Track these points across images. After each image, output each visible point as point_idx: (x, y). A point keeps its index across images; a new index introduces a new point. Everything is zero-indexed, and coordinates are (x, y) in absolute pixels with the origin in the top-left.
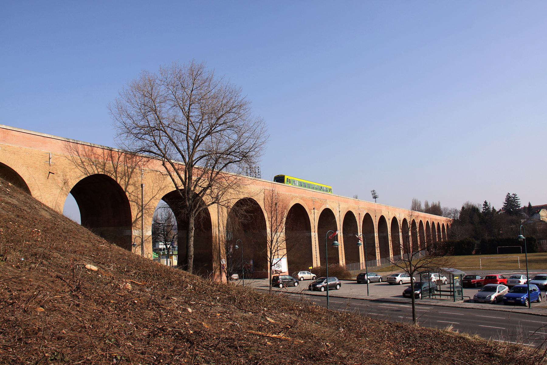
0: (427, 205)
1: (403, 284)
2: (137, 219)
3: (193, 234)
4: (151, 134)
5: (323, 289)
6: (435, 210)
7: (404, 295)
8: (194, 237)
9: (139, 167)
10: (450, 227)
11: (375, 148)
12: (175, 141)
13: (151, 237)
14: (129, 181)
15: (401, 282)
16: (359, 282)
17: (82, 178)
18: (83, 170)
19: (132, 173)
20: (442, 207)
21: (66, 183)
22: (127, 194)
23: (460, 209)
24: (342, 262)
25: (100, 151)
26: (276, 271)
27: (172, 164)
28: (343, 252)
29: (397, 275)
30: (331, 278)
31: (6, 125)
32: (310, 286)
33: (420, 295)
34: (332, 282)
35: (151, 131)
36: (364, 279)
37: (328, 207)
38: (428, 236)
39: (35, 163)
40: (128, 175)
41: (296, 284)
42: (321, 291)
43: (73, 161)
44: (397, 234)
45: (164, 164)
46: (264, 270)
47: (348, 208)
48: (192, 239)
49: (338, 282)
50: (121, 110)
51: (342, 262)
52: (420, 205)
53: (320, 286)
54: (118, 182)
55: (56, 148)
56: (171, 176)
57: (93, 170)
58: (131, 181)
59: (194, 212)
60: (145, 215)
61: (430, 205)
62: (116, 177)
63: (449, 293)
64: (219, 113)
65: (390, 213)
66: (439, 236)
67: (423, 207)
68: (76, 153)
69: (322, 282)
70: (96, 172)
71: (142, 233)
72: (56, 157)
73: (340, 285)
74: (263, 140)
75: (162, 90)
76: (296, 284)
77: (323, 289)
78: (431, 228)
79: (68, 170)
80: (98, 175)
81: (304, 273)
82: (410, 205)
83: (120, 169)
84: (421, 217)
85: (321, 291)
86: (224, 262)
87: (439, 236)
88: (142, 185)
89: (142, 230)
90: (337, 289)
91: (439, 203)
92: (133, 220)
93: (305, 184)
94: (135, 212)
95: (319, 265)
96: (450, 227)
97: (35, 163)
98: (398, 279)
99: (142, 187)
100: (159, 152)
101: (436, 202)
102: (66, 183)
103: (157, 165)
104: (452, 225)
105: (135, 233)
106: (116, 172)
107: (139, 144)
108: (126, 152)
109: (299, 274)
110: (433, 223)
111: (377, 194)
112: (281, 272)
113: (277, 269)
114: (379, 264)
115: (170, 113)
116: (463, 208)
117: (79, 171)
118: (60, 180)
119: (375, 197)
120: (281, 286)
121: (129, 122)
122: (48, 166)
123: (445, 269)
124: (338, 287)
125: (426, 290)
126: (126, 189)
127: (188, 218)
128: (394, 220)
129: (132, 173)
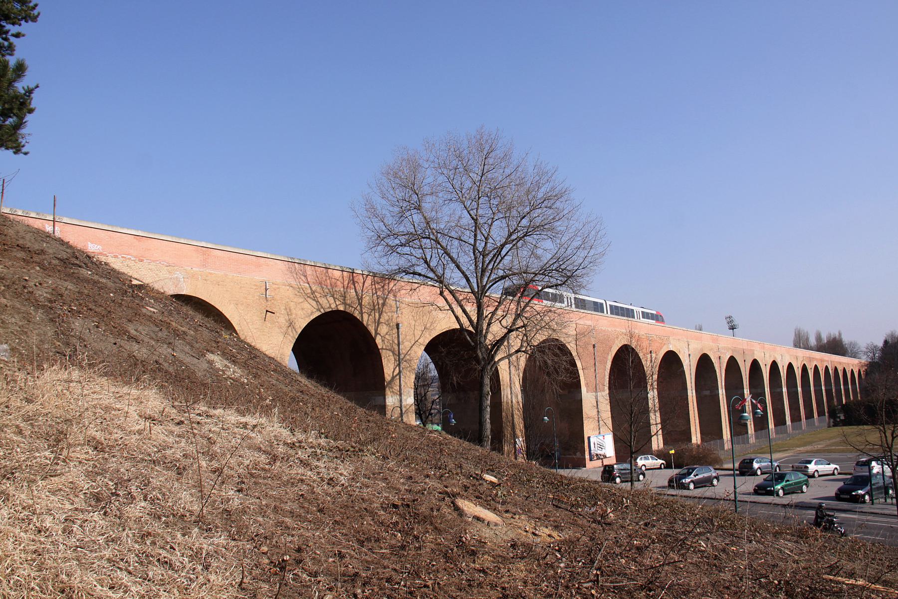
0: (819, 338)
1: (820, 476)
2: (393, 378)
3: (489, 402)
4: (415, 245)
5: (692, 486)
6: (835, 346)
7: (838, 497)
8: (491, 407)
9: (395, 296)
10: (863, 377)
11: (736, 252)
12: (455, 256)
13: (413, 407)
14: (380, 318)
15: (816, 474)
16: (742, 474)
17: (312, 318)
18: (314, 303)
19: (384, 304)
20: (846, 339)
21: (291, 324)
22: (378, 340)
23: (880, 344)
24: (696, 438)
25: (337, 274)
26: (597, 455)
27: (451, 292)
28: (697, 421)
29: (810, 462)
30: (704, 468)
31: (207, 242)
32: (671, 481)
33: (867, 497)
34: (706, 475)
35: (412, 238)
36: (752, 467)
37: (671, 348)
38: (829, 392)
39: (246, 298)
40: (378, 308)
41: (641, 477)
42: (689, 489)
43: (300, 289)
44: (778, 390)
45: (441, 294)
46: (578, 454)
47: (702, 349)
48: (489, 409)
49: (714, 475)
50: (372, 211)
51: (696, 438)
52: (807, 339)
53: (688, 480)
54: (365, 323)
55: (274, 272)
56: (453, 311)
57: (330, 304)
58: (385, 317)
59: (489, 368)
60: (404, 371)
61: (825, 340)
62: (361, 313)
63: (732, 472)
64: (533, 213)
65: (767, 355)
66: (847, 391)
67: (813, 341)
68: (303, 278)
69: (690, 474)
70: (333, 306)
71: (401, 401)
72: (274, 286)
73: (717, 478)
74: (600, 250)
75: (429, 177)
76: (641, 477)
77: (692, 486)
78: (833, 377)
79: (292, 305)
80: (338, 312)
81: (646, 459)
82: (791, 338)
83: (366, 300)
84: (817, 360)
85: (689, 489)
86: (520, 442)
87: (847, 391)
88: (398, 325)
89: (400, 395)
90: (802, 492)
91: (840, 334)
92: (388, 378)
93: (648, 313)
94: (389, 368)
95: (661, 446)
96: (863, 377)
97: (246, 298)
98: (812, 467)
99: (398, 328)
100: (431, 275)
101: (834, 333)
102: (291, 324)
103: (428, 293)
104: (866, 372)
105: (391, 400)
106: (360, 304)
107: (395, 262)
108: (374, 275)
109: (638, 461)
110: (836, 369)
111: (735, 323)
112: (605, 457)
113: (599, 452)
114: (752, 440)
115: (450, 215)
116: (886, 342)
117: (309, 307)
118: (282, 320)
119: (732, 328)
120: (618, 480)
121: (379, 225)
122: (263, 302)
123: (234, 371)
124: (715, 482)
125: (878, 488)
126: (376, 330)
127: (482, 378)
128: (774, 366)
129: (384, 304)
